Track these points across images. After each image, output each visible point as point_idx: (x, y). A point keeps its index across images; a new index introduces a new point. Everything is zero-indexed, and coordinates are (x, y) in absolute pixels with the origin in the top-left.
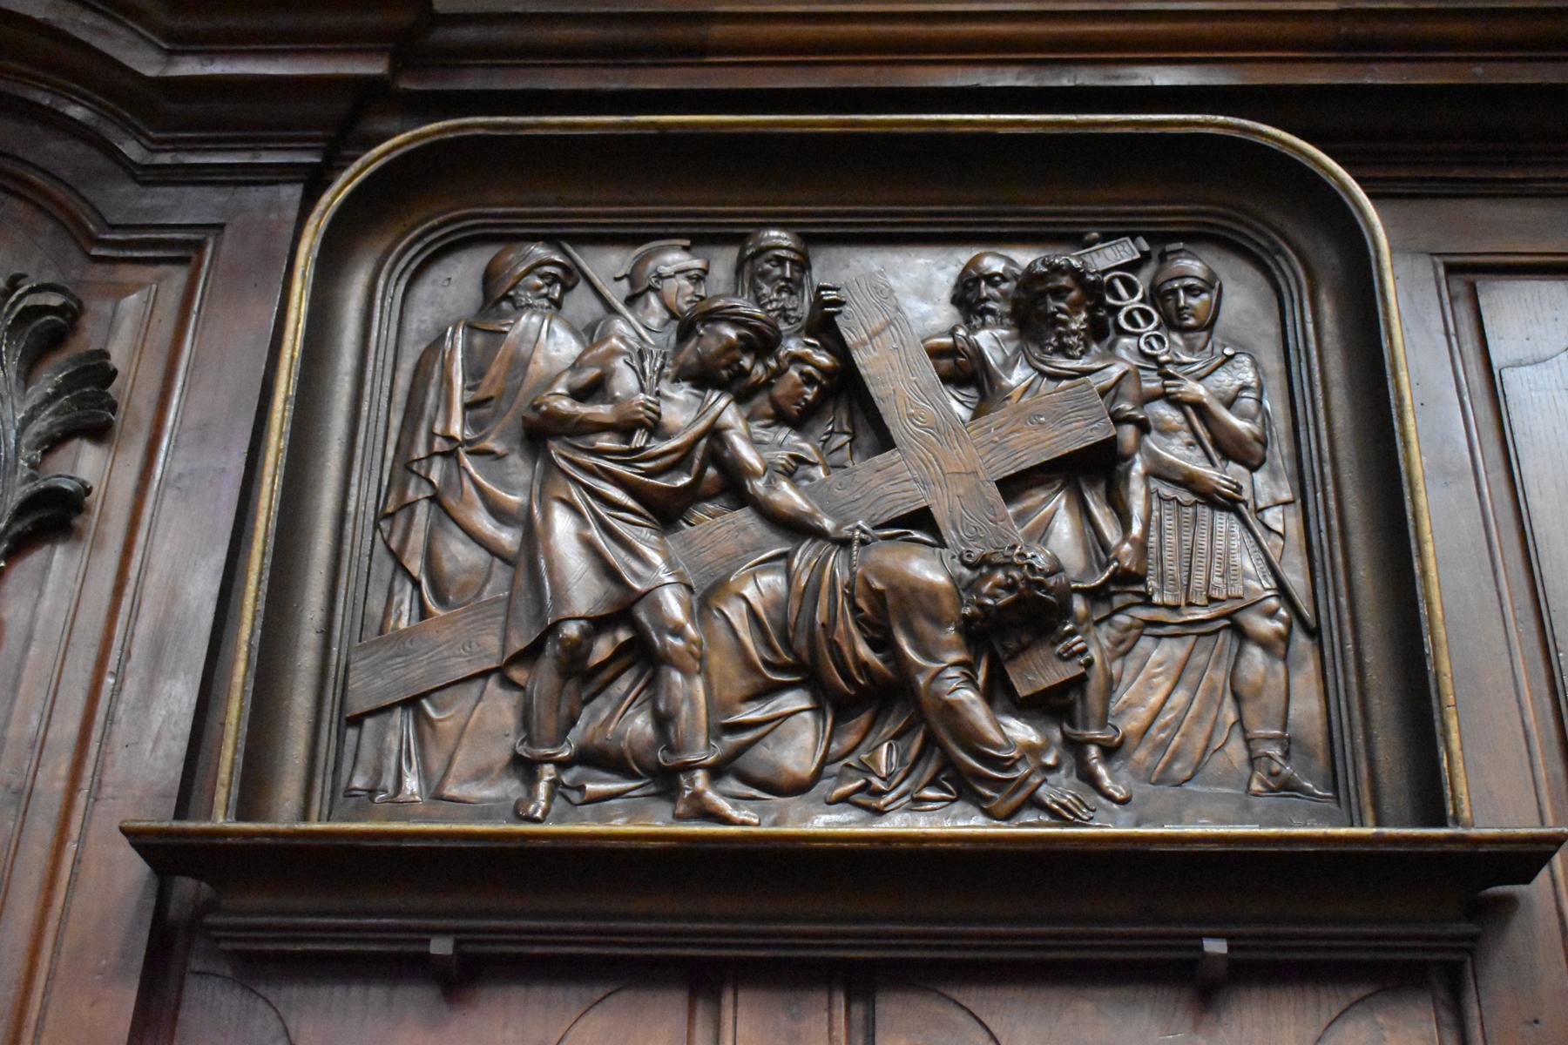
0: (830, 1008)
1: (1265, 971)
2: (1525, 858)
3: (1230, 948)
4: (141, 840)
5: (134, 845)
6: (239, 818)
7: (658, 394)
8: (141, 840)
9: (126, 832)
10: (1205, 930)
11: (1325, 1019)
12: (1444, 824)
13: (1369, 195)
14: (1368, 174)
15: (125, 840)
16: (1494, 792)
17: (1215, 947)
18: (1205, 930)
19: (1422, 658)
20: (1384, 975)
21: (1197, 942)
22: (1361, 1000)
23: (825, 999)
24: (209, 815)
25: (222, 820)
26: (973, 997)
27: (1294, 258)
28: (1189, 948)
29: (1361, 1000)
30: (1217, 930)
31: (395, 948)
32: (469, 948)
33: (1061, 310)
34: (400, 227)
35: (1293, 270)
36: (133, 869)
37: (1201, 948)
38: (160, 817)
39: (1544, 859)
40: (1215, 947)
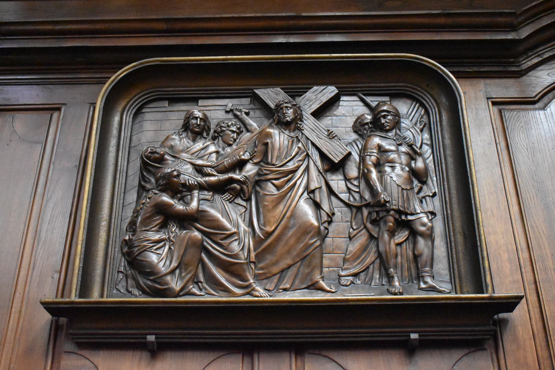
0: (291, 360)
1: (429, 345)
2: (510, 304)
3: (419, 336)
4: (49, 307)
5: (45, 308)
6: (80, 297)
7: (246, 151)
8: (49, 307)
9: (43, 303)
10: (409, 329)
11: (454, 361)
12: (483, 293)
13: (456, 78)
14: (456, 69)
15: (42, 307)
16: (503, 281)
17: (414, 336)
18: (409, 329)
19: (91, 207)
20: (473, 345)
21: (144, 336)
22: (466, 354)
23: (288, 355)
24: (69, 297)
25: (74, 297)
26: (334, 355)
27: (429, 96)
28: (142, 338)
29: (466, 354)
30: (152, 331)
31: (465, 337)
32: (160, 340)
33: (387, 122)
34: (139, 91)
35: (430, 102)
36: (47, 317)
37: (409, 336)
38: (50, 297)
39: (516, 304)
40: (414, 336)
